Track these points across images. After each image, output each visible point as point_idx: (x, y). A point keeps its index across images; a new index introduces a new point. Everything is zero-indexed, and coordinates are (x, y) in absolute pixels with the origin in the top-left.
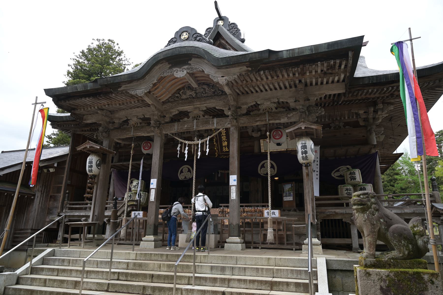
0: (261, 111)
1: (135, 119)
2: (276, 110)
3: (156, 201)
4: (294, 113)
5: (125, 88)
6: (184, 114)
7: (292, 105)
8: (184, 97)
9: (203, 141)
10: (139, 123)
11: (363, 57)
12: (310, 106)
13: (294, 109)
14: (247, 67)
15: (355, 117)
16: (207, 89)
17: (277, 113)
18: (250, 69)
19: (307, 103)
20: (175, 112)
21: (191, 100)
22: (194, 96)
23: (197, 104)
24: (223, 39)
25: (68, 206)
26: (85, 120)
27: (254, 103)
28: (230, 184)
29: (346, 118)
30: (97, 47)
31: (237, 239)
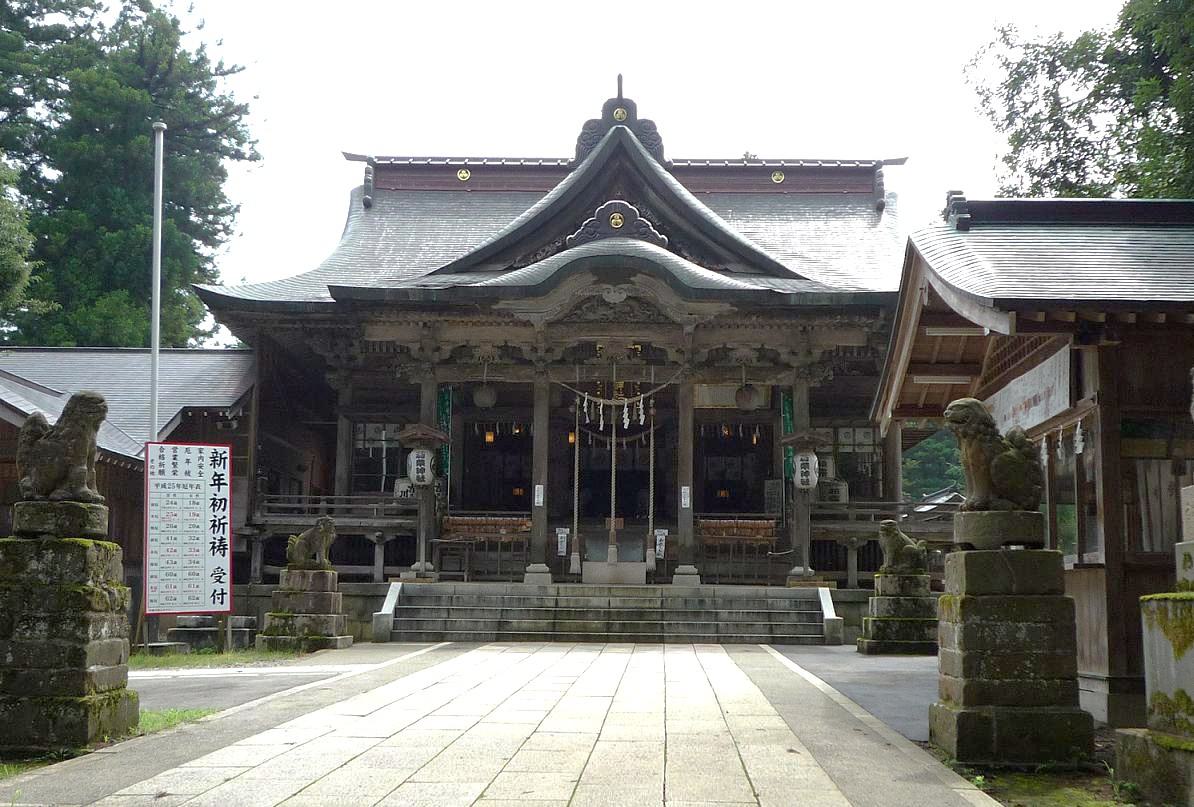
0: (734, 363)
1: (489, 348)
2: (759, 364)
3: (548, 505)
4: (788, 373)
5: (506, 307)
6: (589, 348)
7: (784, 357)
8: (591, 316)
9: (631, 400)
10: (496, 357)
11: (893, 196)
12: (813, 364)
13: (788, 366)
14: (732, 304)
15: (869, 355)
16: (637, 308)
17: (761, 369)
18: (736, 309)
19: (809, 360)
20: (572, 341)
21: (604, 324)
22: (611, 318)
23: (619, 335)
24: (630, 159)
25: (265, 503)
26: (370, 336)
27: (721, 346)
28: (223, 328)
29: (855, 354)
30: (169, 18)
31: (691, 568)
